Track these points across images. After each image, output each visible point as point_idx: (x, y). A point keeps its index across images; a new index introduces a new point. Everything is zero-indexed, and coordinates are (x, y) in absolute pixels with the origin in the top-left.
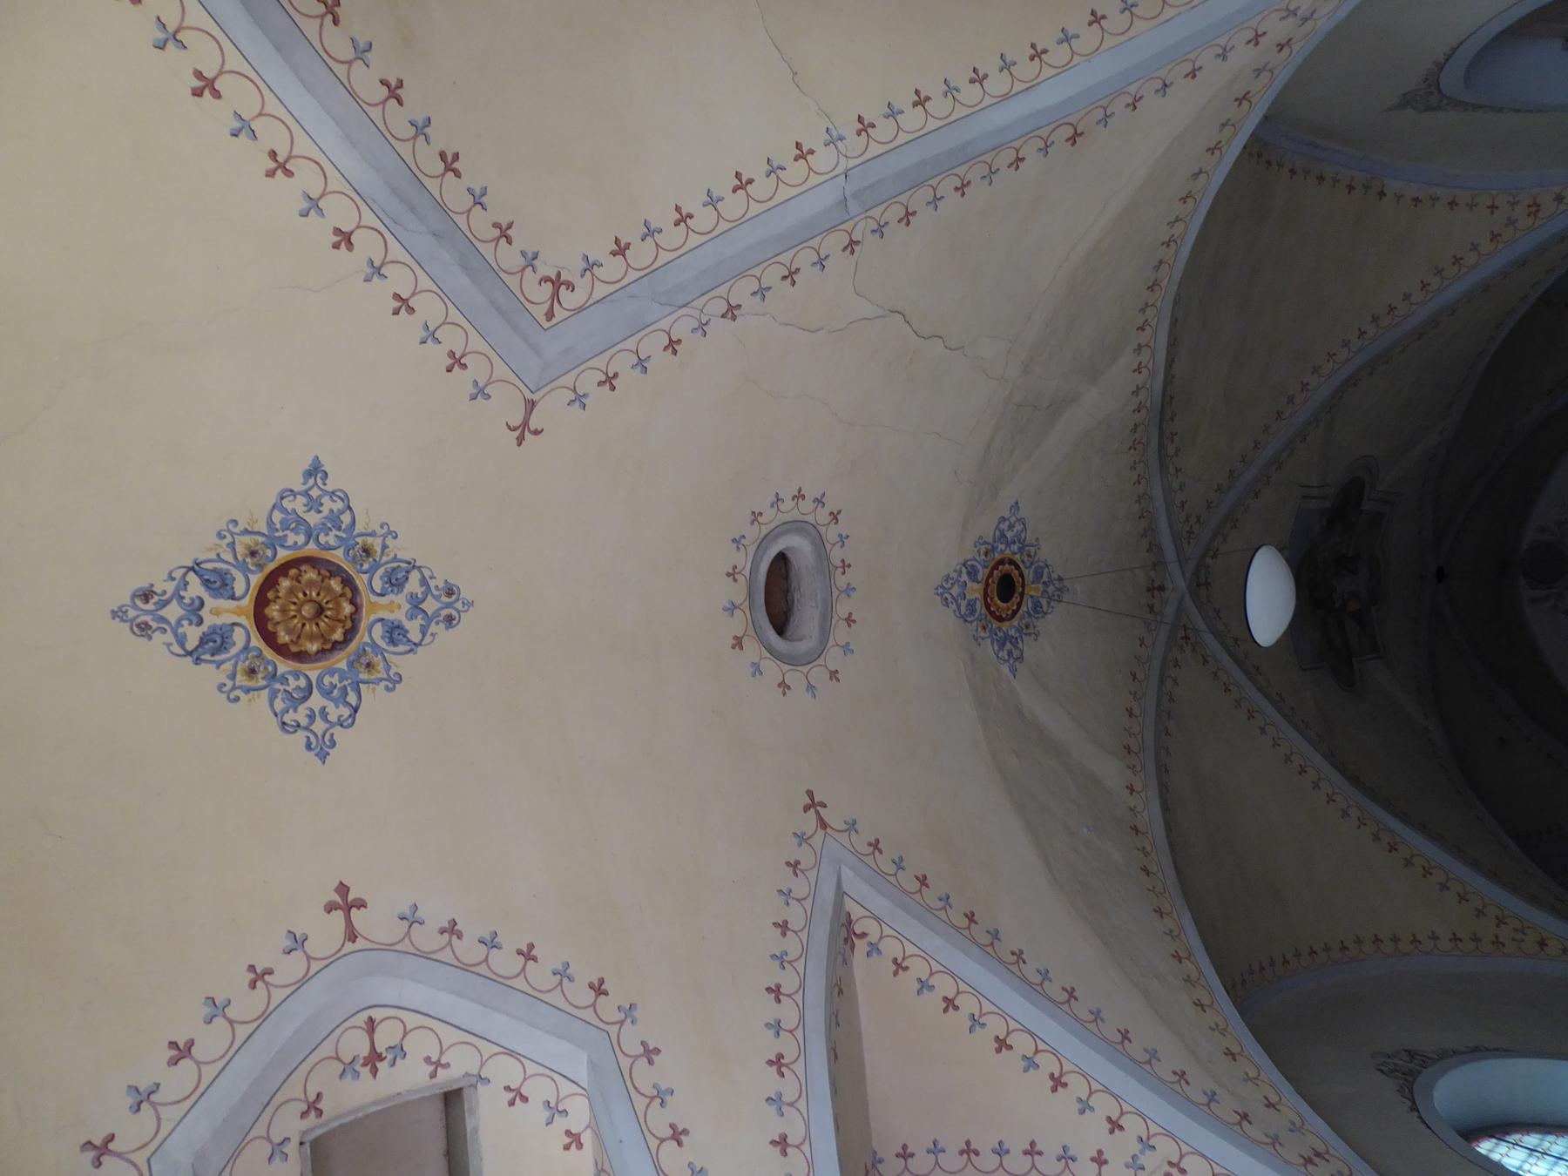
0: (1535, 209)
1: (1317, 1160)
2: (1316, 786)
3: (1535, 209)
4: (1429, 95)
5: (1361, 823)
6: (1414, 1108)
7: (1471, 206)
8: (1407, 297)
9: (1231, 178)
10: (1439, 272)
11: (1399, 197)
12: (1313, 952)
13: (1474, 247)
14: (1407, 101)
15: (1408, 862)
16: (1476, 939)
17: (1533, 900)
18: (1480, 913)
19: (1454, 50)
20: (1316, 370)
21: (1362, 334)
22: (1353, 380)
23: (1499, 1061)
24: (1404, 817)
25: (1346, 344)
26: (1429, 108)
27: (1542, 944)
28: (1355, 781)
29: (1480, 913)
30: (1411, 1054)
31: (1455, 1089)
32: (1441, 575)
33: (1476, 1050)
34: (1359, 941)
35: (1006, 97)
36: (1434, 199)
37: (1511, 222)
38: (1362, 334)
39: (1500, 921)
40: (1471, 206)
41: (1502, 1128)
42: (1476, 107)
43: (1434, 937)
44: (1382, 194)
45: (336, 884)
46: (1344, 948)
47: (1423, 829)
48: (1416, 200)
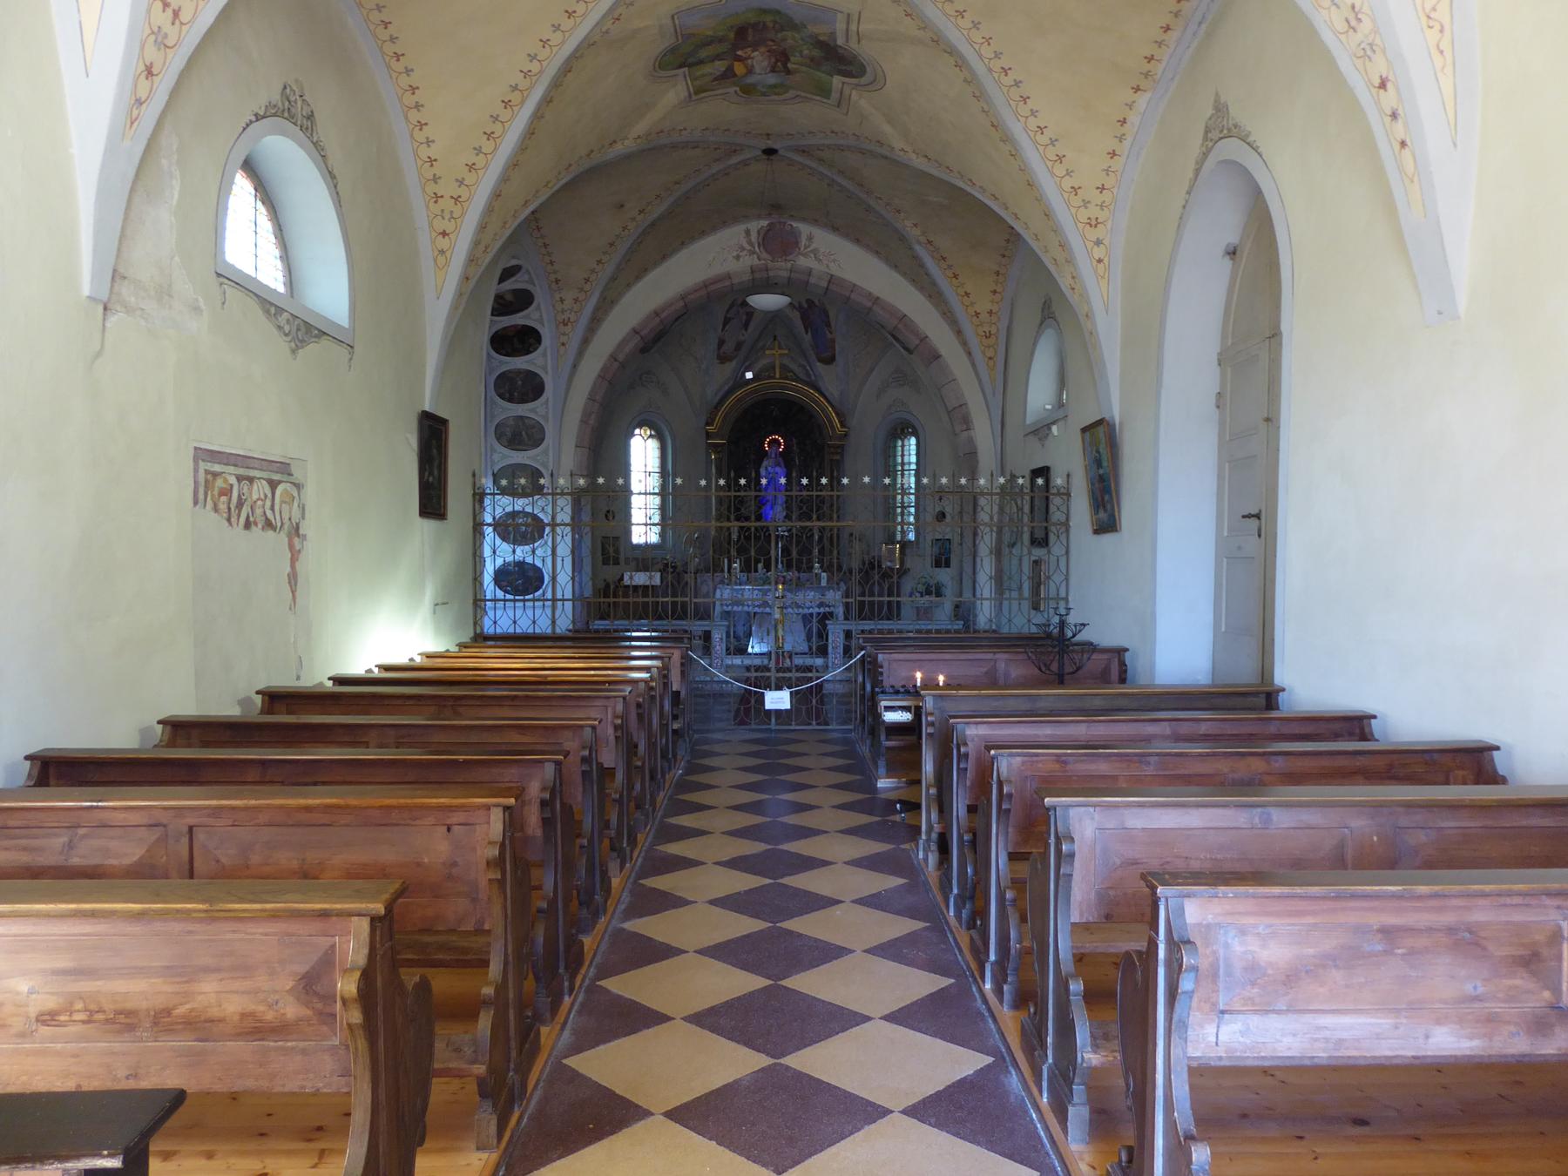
0: (1093, 223)
1: (169, 12)
2: (556, 28)
3: (1093, 223)
4: (1221, 127)
5: (526, 74)
6: (258, 118)
7: (1107, 171)
8: (1033, 113)
9: (628, 516)
10: (1053, 142)
11: (1130, 106)
12: (386, 24)
13: (1069, 173)
14: (1220, 109)
15: (495, 119)
16: (435, 179)
17: (482, 227)
18: (461, 182)
19: (1255, 149)
20: (976, 25)
21: (1005, 71)
22: (961, 63)
23: (326, 192)
24: (537, 116)
25: (997, 55)
26: (1207, 132)
27: (444, 234)
28: (567, 68)
29: (461, 182)
30: (310, 117)
31: (284, 151)
32: (770, 152)
33: (333, 177)
34: (408, 71)
35: (980, 56)
36: (1121, 139)
37: (1086, 204)
38: (1005, 71)
39: (456, 199)
40: (1107, 171)
41: (265, 193)
42: (1197, 172)
43: (429, 142)
44: (1137, 89)
45: (180, 475)
46: (398, 57)
47: (530, 133)
48: (1124, 121)
